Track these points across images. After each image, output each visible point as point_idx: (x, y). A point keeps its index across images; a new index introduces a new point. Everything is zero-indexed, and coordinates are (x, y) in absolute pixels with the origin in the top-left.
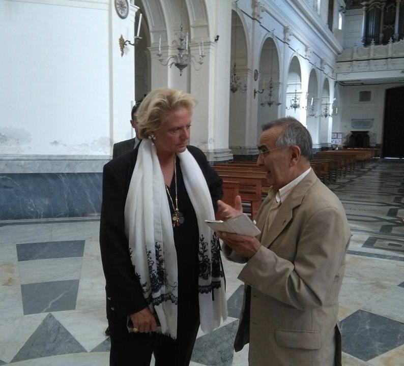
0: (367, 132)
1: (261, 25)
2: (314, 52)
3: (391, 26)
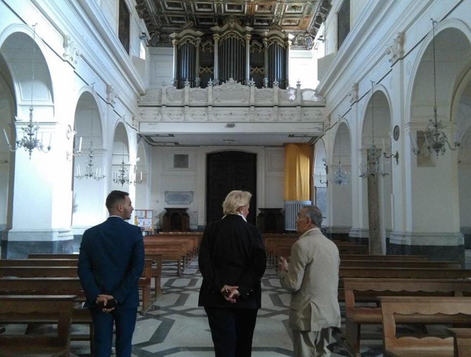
0: (185, 209)
1: (114, 110)
2: (82, 56)
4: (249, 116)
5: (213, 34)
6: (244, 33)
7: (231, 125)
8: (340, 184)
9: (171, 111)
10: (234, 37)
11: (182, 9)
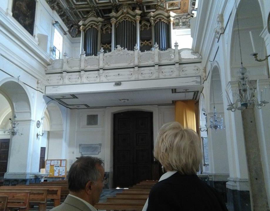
3: (108, 46)
4: (134, 75)
5: (111, 19)
6: (134, 16)
7: (118, 84)
8: (216, 129)
9: (71, 75)
10: (127, 19)
11: (86, 3)
